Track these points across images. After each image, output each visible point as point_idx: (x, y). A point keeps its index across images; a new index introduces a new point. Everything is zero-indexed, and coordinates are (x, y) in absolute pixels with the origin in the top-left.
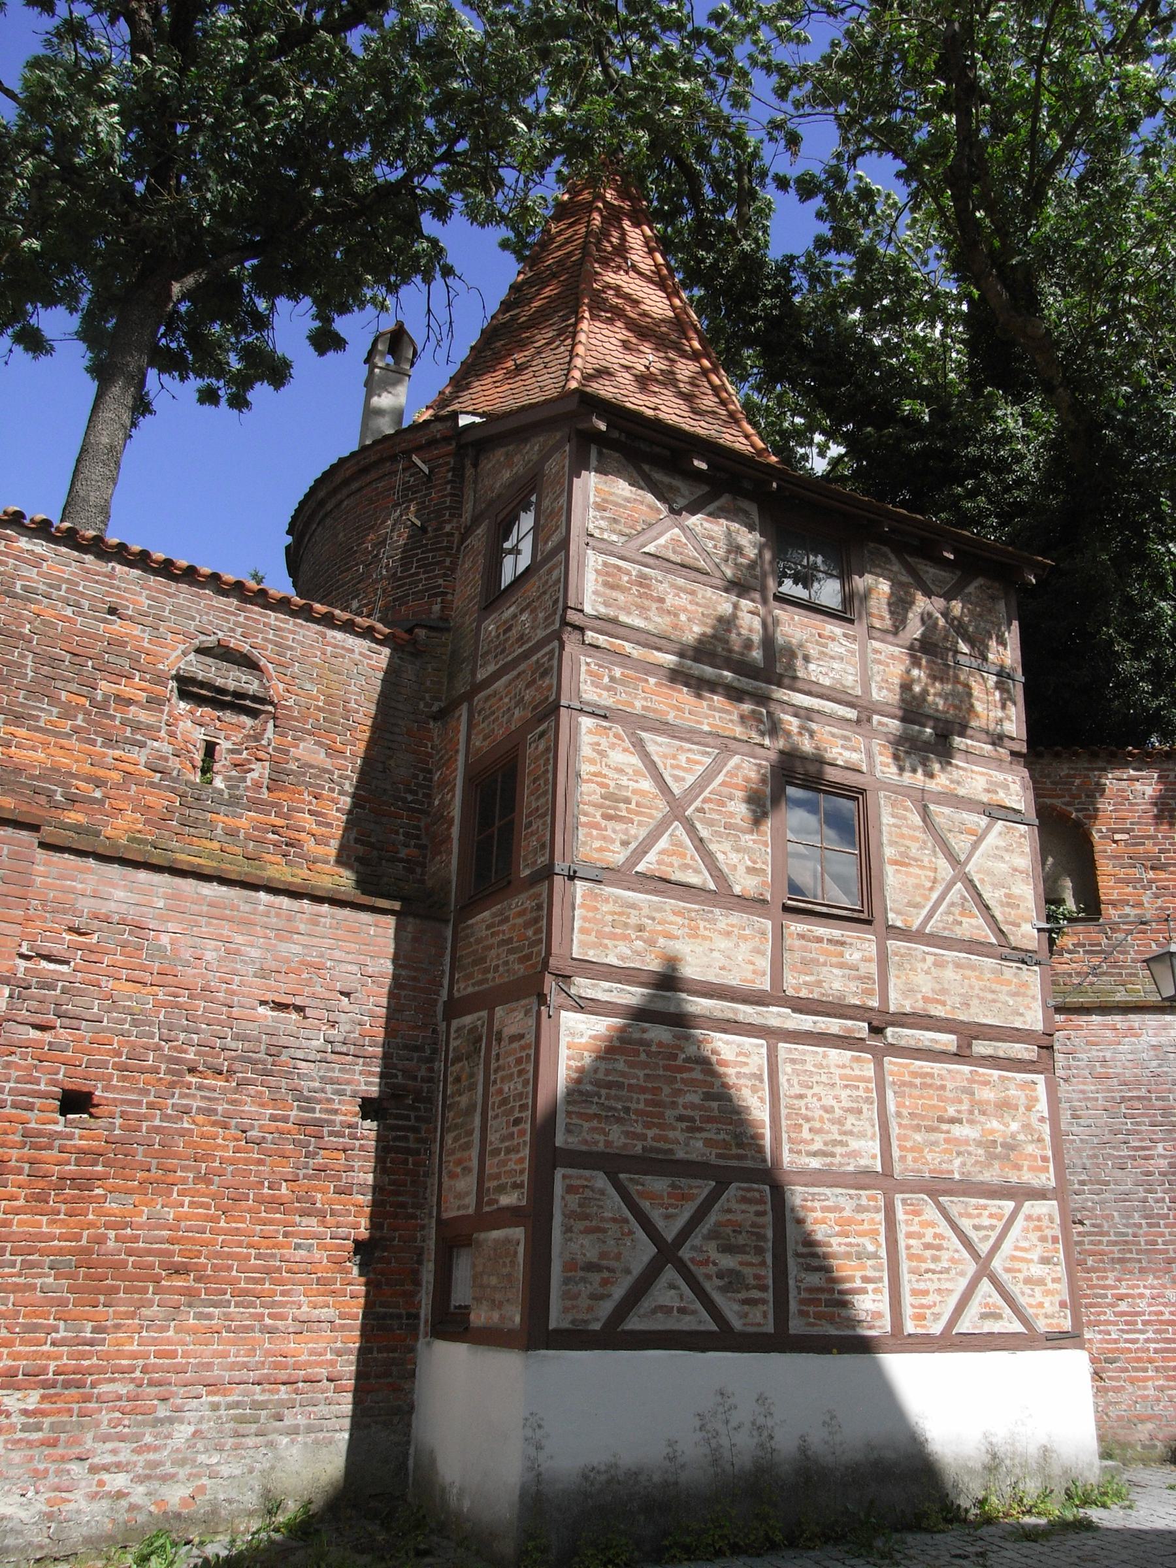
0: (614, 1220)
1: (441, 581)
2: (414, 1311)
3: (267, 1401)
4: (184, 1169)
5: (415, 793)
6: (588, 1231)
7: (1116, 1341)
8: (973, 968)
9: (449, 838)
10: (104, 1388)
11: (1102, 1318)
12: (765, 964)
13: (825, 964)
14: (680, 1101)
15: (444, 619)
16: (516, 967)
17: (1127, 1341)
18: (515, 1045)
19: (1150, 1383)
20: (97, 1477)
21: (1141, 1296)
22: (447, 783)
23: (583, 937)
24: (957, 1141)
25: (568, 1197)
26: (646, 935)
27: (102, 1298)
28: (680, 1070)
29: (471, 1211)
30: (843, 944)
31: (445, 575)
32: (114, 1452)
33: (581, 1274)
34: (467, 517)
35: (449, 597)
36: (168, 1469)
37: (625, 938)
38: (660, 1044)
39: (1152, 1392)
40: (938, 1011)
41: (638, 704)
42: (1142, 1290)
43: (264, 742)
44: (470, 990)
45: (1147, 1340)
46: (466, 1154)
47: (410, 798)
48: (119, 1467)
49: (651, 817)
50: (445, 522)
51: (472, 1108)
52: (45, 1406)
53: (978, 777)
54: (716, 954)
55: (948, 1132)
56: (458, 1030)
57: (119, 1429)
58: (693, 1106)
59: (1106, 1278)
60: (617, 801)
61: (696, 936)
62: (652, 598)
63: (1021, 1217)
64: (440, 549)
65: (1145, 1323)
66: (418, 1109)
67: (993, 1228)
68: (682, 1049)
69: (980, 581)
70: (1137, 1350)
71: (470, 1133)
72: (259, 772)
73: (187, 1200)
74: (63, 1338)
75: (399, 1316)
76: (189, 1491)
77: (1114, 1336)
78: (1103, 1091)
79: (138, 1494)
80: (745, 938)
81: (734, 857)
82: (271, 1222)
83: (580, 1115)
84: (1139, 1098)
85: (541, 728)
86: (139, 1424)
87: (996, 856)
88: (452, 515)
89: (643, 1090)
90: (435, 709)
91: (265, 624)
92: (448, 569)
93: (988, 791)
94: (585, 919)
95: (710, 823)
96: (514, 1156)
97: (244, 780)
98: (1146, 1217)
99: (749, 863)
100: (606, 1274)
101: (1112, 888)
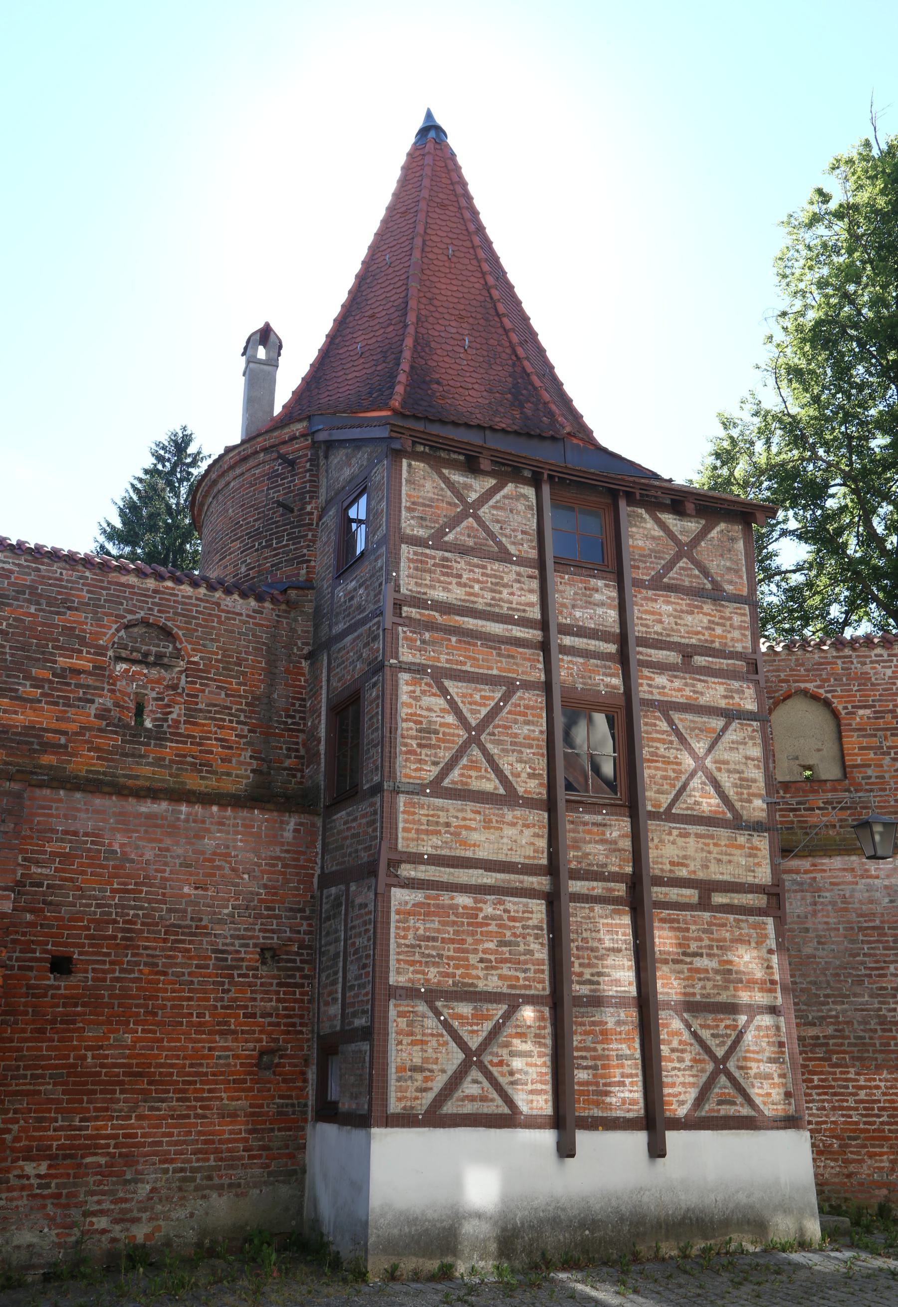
0: (432, 1035)
1: (305, 551)
2: (303, 1101)
3: (200, 1167)
4: (137, 1006)
5: (293, 717)
6: (413, 1043)
7: (857, 1123)
8: (712, 837)
9: (318, 753)
10: (89, 1160)
11: (845, 1104)
12: (543, 843)
13: (590, 842)
14: (480, 947)
15: (309, 580)
16: (363, 854)
17: (865, 1123)
18: (363, 911)
19: (885, 1157)
20: (88, 1220)
21: (878, 1087)
22: (315, 711)
23: (405, 834)
24: (698, 971)
25: (399, 1020)
26: (452, 829)
27: (85, 1098)
28: (481, 925)
29: (338, 1028)
30: (605, 825)
31: (309, 546)
32: (99, 1202)
33: (409, 1073)
34: (322, 499)
35: (313, 564)
36: (135, 1214)
37: (438, 833)
38: (464, 907)
39: (887, 1164)
40: (683, 873)
41: (443, 657)
42: (877, 1083)
43: (180, 691)
44: (334, 868)
45: (882, 1123)
46: (334, 988)
47: (290, 721)
48: (102, 1213)
49: (453, 742)
50: (306, 503)
51: (337, 955)
52: (52, 1171)
53: (717, 687)
54: (505, 840)
55: (691, 963)
56: (327, 897)
57: (101, 1187)
58: (492, 952)
59: (848, 1073)
60: (429, 733)
61: (489, 828)
62: (453, 576)
63: (752, 1027)
64: (304, 525)
65: (880, 1109)
66: (302, 954)
67: (728, 1036)
68: (481, 910)
69: (722, 526)
70: (874, 1130)
71: (336, 973)
72: (177, 712)
73: (140, 1028)
74: (61, 1126)
75: (293, 1105)
76: (150, 1230)
77: (855, 1119)
78: (844, 922)
79: (117, 1230)
80: (527, 826)
81: (519, 767)
82: (200, 1041)
83: (406, 962)
84: (873, 928)
85: (374, 680)
86: (114, 1184)
87: (731, 749)
88: (311, 498)
89: (452, 941)
90: (305, 652)
91: (175, 602)
92: (310, 541)
93: (725, 697)
94: (406, 821)
95: (498, 742)
96: (363, 991)
97: (166, 720)
98: (881, 1024)
99: (529, 770)
100: (428, 1074)
101: (857, 755)
